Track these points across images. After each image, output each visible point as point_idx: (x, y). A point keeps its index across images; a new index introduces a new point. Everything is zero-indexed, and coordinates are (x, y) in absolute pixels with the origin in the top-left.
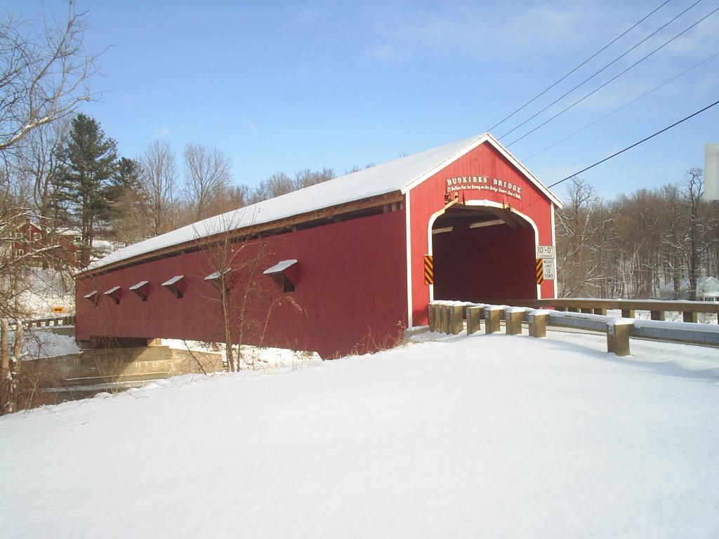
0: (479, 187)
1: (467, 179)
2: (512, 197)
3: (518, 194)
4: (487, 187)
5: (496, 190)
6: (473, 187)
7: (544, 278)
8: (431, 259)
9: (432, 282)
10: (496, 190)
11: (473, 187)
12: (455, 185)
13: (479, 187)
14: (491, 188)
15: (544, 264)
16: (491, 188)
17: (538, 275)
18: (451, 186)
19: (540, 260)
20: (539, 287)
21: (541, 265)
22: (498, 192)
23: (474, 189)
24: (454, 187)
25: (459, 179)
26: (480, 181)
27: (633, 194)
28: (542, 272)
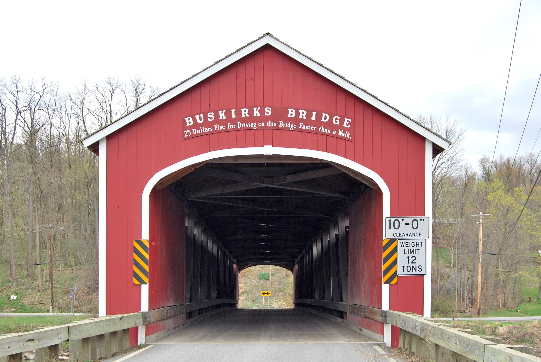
0: (254, 126)
1: (228, 114)
2: (331, 135)
3: (345, 130)
4: (270, 124)
5: (292, 127)
6: (240, 125)
7: (400, 272)
8: (147, 244)
9: (146, 280)
10: (292, 127)
11: (240, 125)
12: (201, 125)
13: (254, 126)
14: (281, 124)
15: (401, 249)
16: (281, 124)
17: (384, 255)
18: (190, 128)
19: (392, 241)
20: (386, 288)
21: (395, 250)
22: (296, 130)
23: (241, 129)
24: (197, 129)
25: (211, 116)
26: (256, 113)
27: (266, 154)
28: (395, 262)
